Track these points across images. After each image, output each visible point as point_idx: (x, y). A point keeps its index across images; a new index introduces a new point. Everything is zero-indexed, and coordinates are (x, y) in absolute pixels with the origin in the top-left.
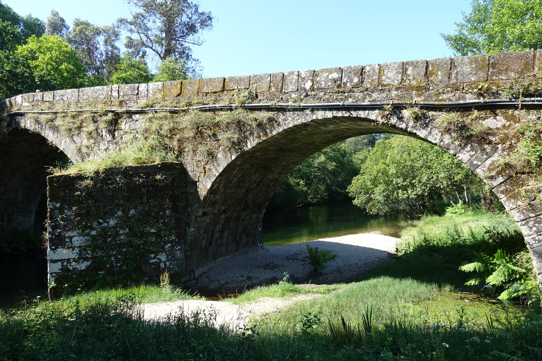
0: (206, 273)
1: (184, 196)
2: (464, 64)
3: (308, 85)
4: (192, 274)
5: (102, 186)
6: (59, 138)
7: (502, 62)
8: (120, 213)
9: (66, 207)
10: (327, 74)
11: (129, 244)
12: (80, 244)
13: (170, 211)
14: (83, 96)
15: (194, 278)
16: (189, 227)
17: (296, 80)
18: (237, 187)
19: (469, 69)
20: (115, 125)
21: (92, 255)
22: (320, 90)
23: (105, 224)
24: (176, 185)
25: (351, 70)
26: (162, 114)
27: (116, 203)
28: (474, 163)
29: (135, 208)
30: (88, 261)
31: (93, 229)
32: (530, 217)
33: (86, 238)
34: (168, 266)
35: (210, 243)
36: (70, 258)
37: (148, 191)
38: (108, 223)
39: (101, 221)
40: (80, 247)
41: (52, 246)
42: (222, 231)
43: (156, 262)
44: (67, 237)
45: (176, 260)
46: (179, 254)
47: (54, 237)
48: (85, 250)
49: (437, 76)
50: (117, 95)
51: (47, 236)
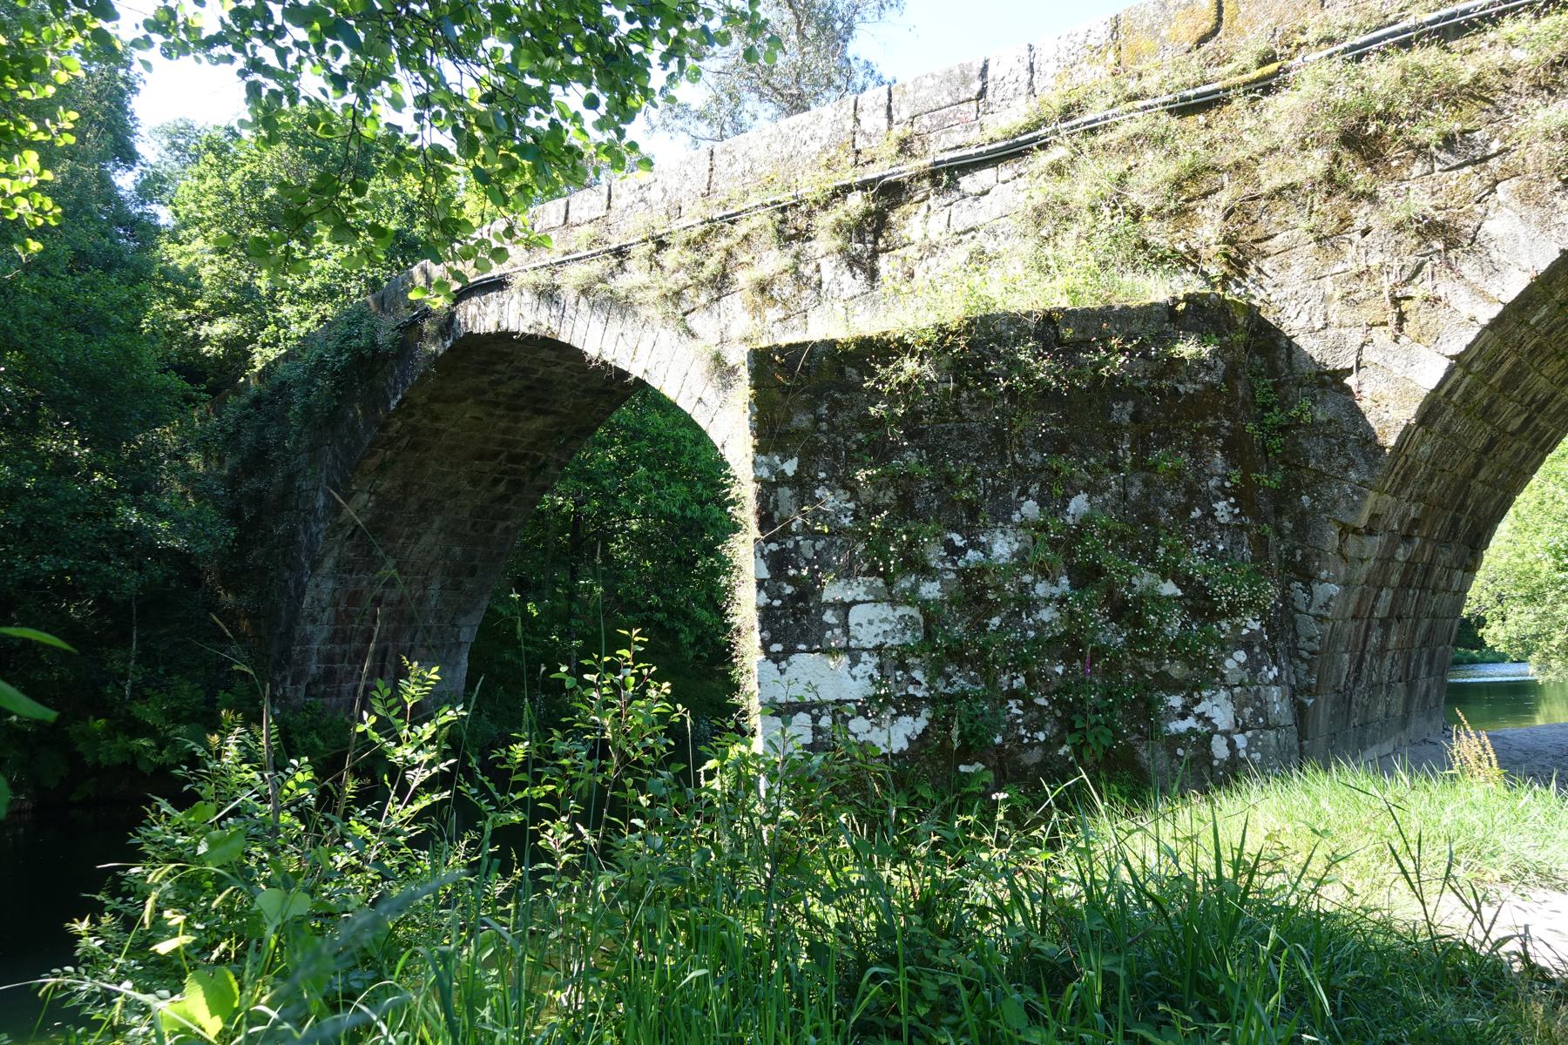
1: (1275, 443)
6: (630, 336)
9: (822, 475)
11: (1070, 645)
12: (881, 639)
20: (877, 234)
27: (1015, 463)
29: (1092, 489)
30: (916, 715)
36: (845, 696)
38: (985, 549)
40: (878, 649)
41: (774, 640)
44: (828, 605)
45: (1272, 729)
47: (777, 603)
48: (903, 666)
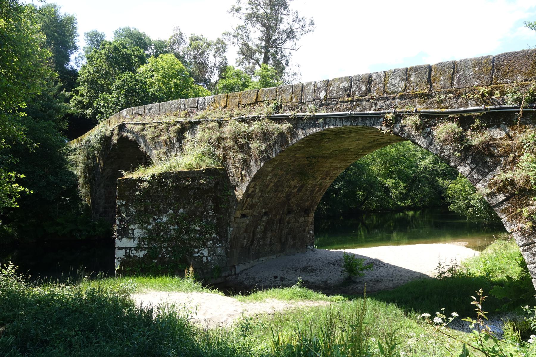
0: (247, 270)
1: (226, 198)
2: (467, 67)
3: (322, 95)
4: (233, 270)
5: (158, 188)
7: (507, 62)
10: (339, 83)
11: (176, 238)
15: (235, 274)
17: (313, 90)
18: (276, 191)
19: (472, 73)
21: (148, 246)
22: (333, 100)
23: (159, 221)
24: (218, 188)
25: (359, 78)
26: (211, 125)
27: (169, 202)
28: (475, 177)
31: (150, 224)
33: (144, 231)
35: (252, 243)
37: (194, 193)
38: (161, 219)
40: (139, 238)
41: (119, 236)
42: (265, 232)
43: (199, 256)
44: (130, 229)
46: (219, 251)
49: (439, 81)
50: (184, 108)
51: (116, 227)
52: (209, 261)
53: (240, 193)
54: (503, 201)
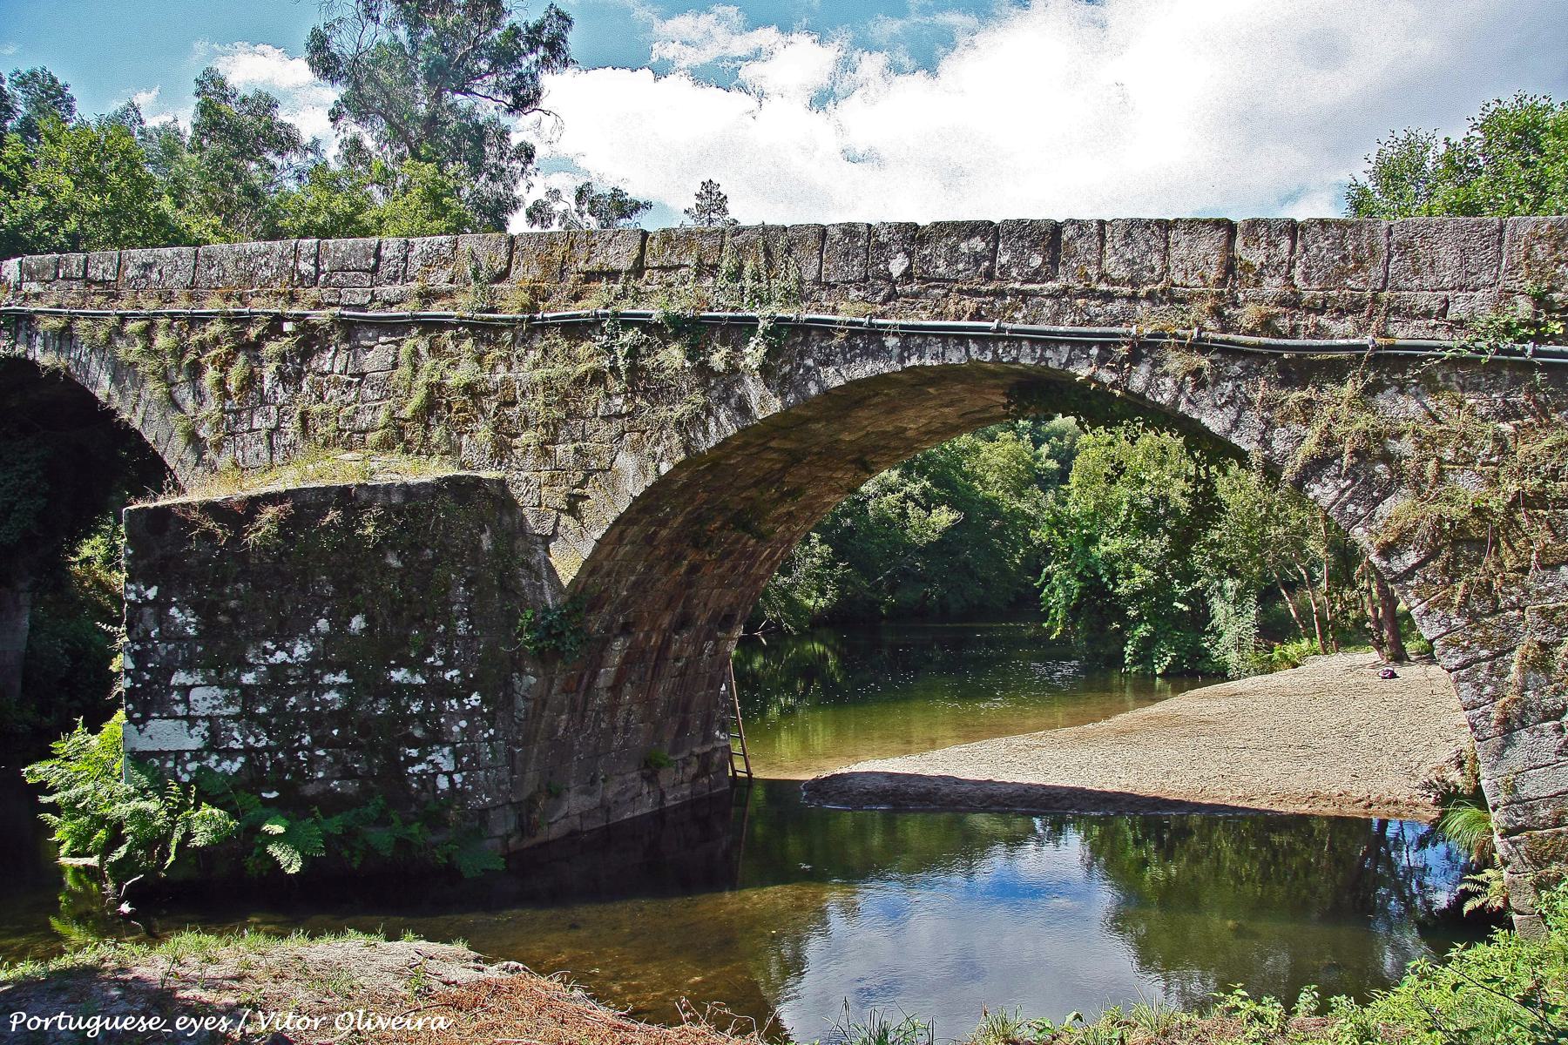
8: (323, 624)
13: (468, 624)
14: (209, 268)
16: (522, 672)
23: (281, 656)
31: (251, 667)
32: (1479, 660)
34: (459, 786)
38: (290, 653)
39: (269, 645)
42: (615, 689)
44: (175, 688)
50: (313, 269)
52: (459, 786)
53: (567, 563)
54: (1415, 566)
